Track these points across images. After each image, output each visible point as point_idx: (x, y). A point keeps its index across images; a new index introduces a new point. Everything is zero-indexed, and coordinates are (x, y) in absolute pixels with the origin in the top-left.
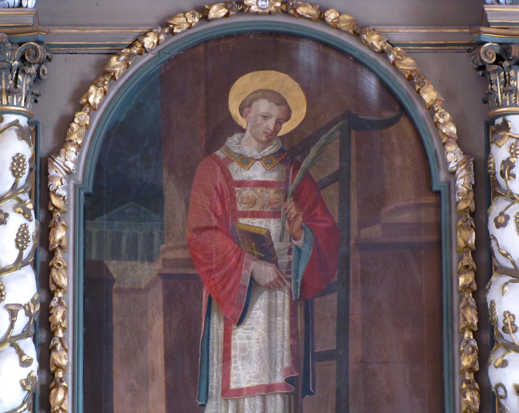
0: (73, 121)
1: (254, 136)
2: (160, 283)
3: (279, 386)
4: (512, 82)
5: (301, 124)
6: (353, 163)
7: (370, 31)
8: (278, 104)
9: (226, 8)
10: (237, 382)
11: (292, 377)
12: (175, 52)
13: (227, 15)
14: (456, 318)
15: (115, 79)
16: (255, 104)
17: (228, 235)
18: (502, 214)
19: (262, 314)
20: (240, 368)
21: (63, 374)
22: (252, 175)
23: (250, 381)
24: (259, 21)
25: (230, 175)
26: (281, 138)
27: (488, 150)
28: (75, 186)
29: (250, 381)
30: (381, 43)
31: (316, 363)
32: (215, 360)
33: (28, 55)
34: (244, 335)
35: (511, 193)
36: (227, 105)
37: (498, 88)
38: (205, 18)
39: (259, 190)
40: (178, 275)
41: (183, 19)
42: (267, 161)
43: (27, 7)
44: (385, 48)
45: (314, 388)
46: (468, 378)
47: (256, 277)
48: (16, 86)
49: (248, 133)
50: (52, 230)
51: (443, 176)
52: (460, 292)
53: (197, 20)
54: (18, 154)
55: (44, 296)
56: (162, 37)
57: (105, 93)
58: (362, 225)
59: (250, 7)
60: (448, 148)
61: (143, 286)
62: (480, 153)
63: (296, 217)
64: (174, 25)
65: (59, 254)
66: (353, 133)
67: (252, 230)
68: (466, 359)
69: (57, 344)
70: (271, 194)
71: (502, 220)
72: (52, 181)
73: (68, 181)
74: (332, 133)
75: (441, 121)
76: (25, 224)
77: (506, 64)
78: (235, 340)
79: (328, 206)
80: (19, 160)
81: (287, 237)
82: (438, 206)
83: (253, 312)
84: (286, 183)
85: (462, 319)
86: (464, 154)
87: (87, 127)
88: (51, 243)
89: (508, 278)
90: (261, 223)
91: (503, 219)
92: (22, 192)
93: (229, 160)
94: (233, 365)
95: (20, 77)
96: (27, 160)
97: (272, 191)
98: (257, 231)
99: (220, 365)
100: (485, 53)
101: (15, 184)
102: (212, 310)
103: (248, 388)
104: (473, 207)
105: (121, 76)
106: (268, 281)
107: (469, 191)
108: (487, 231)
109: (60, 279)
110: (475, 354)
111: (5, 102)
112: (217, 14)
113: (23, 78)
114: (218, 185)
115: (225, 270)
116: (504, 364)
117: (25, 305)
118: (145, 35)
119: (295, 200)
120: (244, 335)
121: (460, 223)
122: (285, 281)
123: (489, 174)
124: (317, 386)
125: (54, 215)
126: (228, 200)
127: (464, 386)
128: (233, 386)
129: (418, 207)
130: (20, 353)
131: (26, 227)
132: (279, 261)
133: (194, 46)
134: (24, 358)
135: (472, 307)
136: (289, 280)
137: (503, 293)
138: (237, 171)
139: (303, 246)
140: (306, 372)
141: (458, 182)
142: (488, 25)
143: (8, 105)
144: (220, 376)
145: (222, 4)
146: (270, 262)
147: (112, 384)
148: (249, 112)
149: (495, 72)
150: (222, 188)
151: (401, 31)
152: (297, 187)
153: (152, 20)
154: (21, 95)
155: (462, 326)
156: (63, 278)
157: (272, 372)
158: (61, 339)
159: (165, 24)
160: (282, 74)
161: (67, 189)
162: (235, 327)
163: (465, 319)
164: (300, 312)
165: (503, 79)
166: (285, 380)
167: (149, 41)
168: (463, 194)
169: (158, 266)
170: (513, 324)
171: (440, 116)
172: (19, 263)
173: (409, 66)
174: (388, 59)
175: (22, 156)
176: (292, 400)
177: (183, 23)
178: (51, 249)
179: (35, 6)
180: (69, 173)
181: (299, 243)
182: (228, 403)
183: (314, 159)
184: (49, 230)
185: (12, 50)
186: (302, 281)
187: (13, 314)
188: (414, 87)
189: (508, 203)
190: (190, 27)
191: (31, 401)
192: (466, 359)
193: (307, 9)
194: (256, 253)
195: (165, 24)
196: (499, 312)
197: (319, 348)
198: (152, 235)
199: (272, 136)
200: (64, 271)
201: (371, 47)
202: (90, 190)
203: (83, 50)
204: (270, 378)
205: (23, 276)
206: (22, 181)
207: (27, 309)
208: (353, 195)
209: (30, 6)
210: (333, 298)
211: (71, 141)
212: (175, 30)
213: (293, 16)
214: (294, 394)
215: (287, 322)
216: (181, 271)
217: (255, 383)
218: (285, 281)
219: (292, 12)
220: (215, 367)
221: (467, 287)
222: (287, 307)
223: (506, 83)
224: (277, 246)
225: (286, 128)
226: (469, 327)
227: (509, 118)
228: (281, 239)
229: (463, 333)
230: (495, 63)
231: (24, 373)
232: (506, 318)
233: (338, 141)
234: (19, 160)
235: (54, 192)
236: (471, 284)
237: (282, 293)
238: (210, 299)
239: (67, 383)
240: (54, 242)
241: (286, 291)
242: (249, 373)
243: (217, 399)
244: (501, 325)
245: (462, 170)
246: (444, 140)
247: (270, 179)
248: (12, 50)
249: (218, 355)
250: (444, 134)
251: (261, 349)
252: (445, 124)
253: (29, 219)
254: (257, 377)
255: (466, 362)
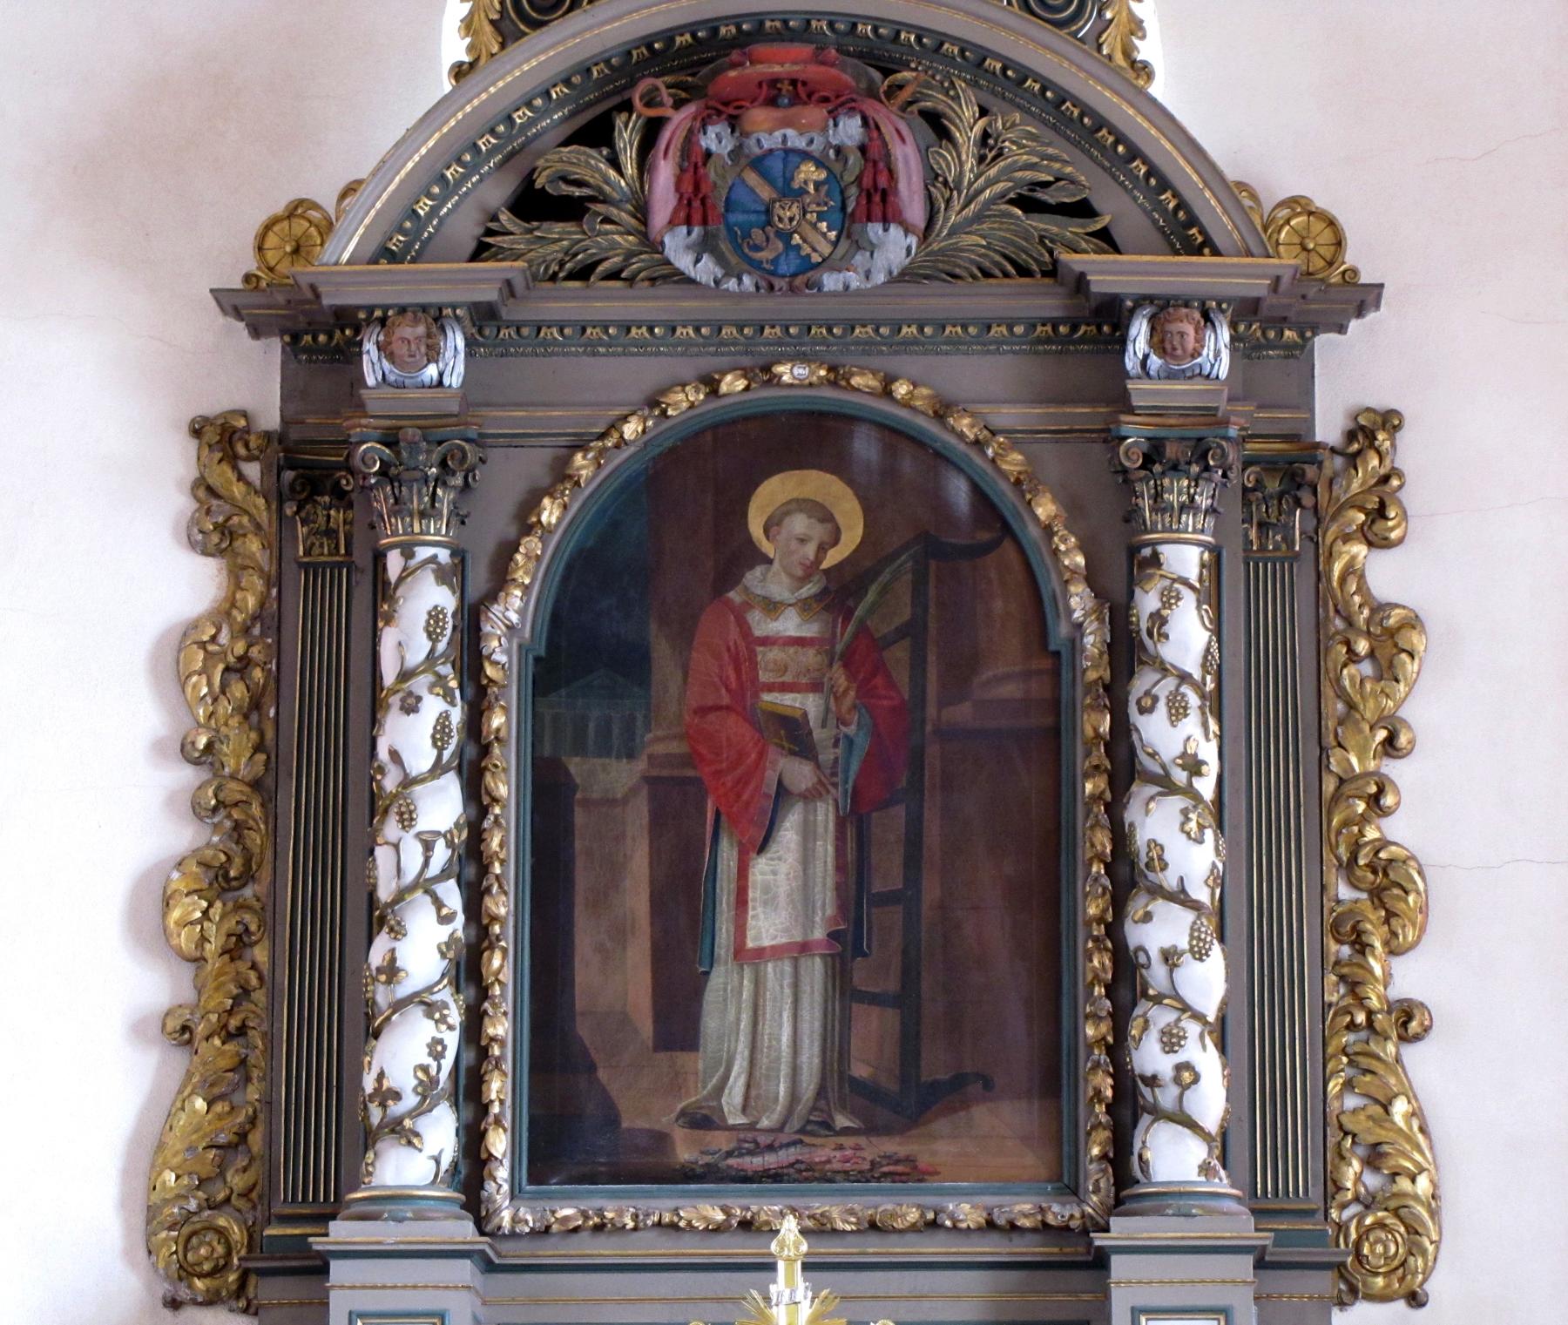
0: (517, 550)
1: (785, 568)
2: (644, 792)
3: (818, 943)
4: (1166, 496)
5: (855, 551)
6: (932, 610)
7: (958, 412)
8: (822, 521)
9: (746, 377)
10: (756, 938)
11: (838, 931)
12: (669, 444)
13: (747, 389)
14: (1080, 842)
15: (579, 486)
16: (787, 521)
17: (746, 720)
18: (1147, 693)
19: (795, 837)
20: (762, 916)
21: (501, 927)
22: (781, 628)
23: (776, 937)
24: (795, 397)
25: (750, 628)
26: (827, 572)
27: (1131, 595)
28: (520, 646)
29: (776, 937)
30: (975, 430)
31: (874, 910)
32: (724, 905)
33: (452, 457)
34: (767, 868)
35: (1162, 662)
36: (746, 524)
37: (1146, 503)
38: (714, 392)
39: (792, 650)
40: (672, 778)
41: (681, 396)
42: (804, 606)
43: (450, 386)
44: (981, 437)
45: (869, 947)
46: (1095, 933)
47: (787, 782)
48: (433, 505)
49: (776, 565)
50: (486, 714)
51: (1064, 630)
52: (1086, 804)
53: (702, 397)
54: (436, 607)
55: (473, 811)
56: (650, 423)
57: (565, 507)
58: (942, 705)
59: (781, 377)
60: (1072, 589)
61: (619, 796)
62: (1122, 599)
63: (846, 691)
64: (668, 405)
65: (496, 750)
66: (933, 564)
67: (780, 710)
68: (1094, 906)
69: (492, 885)
70: (810, 657)
71: (1147, 702)
72: (486, 640)
73: (509, 641)
74: (901, 565)
75: (1062, 547)
76: (446, 712)
77: (1157, 468)
78: (754, 874)
79: (894, 674)
80: (437, 615)
81: (832, 721)
82: (1056, 673)
83: (782, 833)
84: (832, 641)
85: (1088, 844)
86: (1096, 597)
87: (538, 558)
88: (484, 733)
89: (1155, 789)
90: (794, 700)
91: (1149, 702)
92: (443, 663)
93: (748, 606)
94: (751, 913)
95: (439, 492)
96: (449, 615)
97: (811, 652)
98: (788, 712)
99: (733, 913)
100: (1126, 453)
101: (432, 651)
102: (721, 831)
103: (773, 947)
104: (1107, 675)
105: (589, 481)
106: (803, 787)
107: (1101, 654)
108: (1127, 716)
109: (497, 787)
110: (1108, 896)
111: (417, 529)
112: (732, 388)
113: (444, 493)
114: (731, 644)
115: (739, 771)
116: (1148, 917)
117: (446, 832)
118: (625, 419)
119: (846, 666)
120: (767, 868)
121: (1088, 701)
122: (830, 788)
123: (1132, 632)
124: (875, 944)
125: (489, 691)
126: (745, 666)
127: (1090, 944)
128: (750, 944)
129: (1027, 675)
130: (438, 904)
131: (447, 717)
132: (820, 757)
133: (698, 434)
134: (444, 911)
135: (1102, 827)
136: (835, 785)
137: (1147, 812)
138: (759, 621)
139: (857, 734)
140: (858, 923)
141: (1085, 640)
142: (1131, 410)
143: (421, 533)
144: (732, 929)
145: (739, 372)
146: (807, 758)
147: (573, 942)
148: (779, 533)
149: (1141, 480)
150: (736, 648)
151: (1005, 411)
152: (848, 647)
153: (637, 395)
154: (441, 519)
155: (1089, 855)
156: (501, 785)
157: (808, 923)
158: (497, 877)
159: (653, 403)
160: (828, 476)
161: (508, 652)
162: (754, 855)
163: (1093, 845)
164: (850, 833)
165: (1153, 491)
166: (828, 935)
167: (631, 429)
168: (1092, 659)
169: (641, 765)
170: (1160, 858)
171: (1060, 540)
172: (438, 769)
173: (1016, 465)
174: (984, 454)
175: (443, 609)
176: (838, 965)
177: (682, 401)
178: (484, 742)
179: (462, 386)
180: (511, 628)
181: (851, 730)
182: (743, 970)
183: (873, 604)
184: (481, 714)
185: (429, 452)
186: (854, 788)
187: (428, 847)
188: (1024, 496)
189: (1157, 676)
190: (692, 406)
191: (453, 972)
192: (1094, 906)
193: (865, 379)
194: (786, 745)
195: (653, 403)
196: (1142, 837)
197: (878, 886)
198: (633, 718)
199: (811, 569)
200: (502, 775)
201: (961, 436)
202: (542, 653)
203: (533, 441)
204: (805, 933)
205: (442, 789)
206: (442, 646)
207: (448, 837)
208: (932, 658)
209: (454, 385)
210: (899, 812)
211: (514, 580)
212: (670, 412)
213: (845, 388)
214: (841, 955)
215: (830, 849)
216: (676, 773)
217: (783, 940)
218: (830, 788)
219: (843, 383)
220: (725, 916)
221: (1097, 798)
222: (831, 826)
223: (1157, 496)
224: (818, 734)
225: (833, 558)
226: (1100, 857)
227: (1161, 548)
228: (824, 725)
229: (1091, 865)
230: (1142, 467)
231: (443, 933)
232: (1150, 850)
233: (909, 576)
234: (437, 615)
235: (489, 657)
236: (1103, 792)
237: (824, 806)
238: (718, 814)
239: (507, 943)
240: (489, 733)
241: (831, 802)
242: (775, 924)
243: (726, 963)
244: (1144, 859)
245: (1092, 621)
246: (1067, 576)
247: (809, 635)
248: (429, 452)
249: (728, 899)
250: (1066, 567)
251: (792, 889)
252: (1068, 551)
253: (453, 704)
254: (786, 930)
255: (1092, 911)
